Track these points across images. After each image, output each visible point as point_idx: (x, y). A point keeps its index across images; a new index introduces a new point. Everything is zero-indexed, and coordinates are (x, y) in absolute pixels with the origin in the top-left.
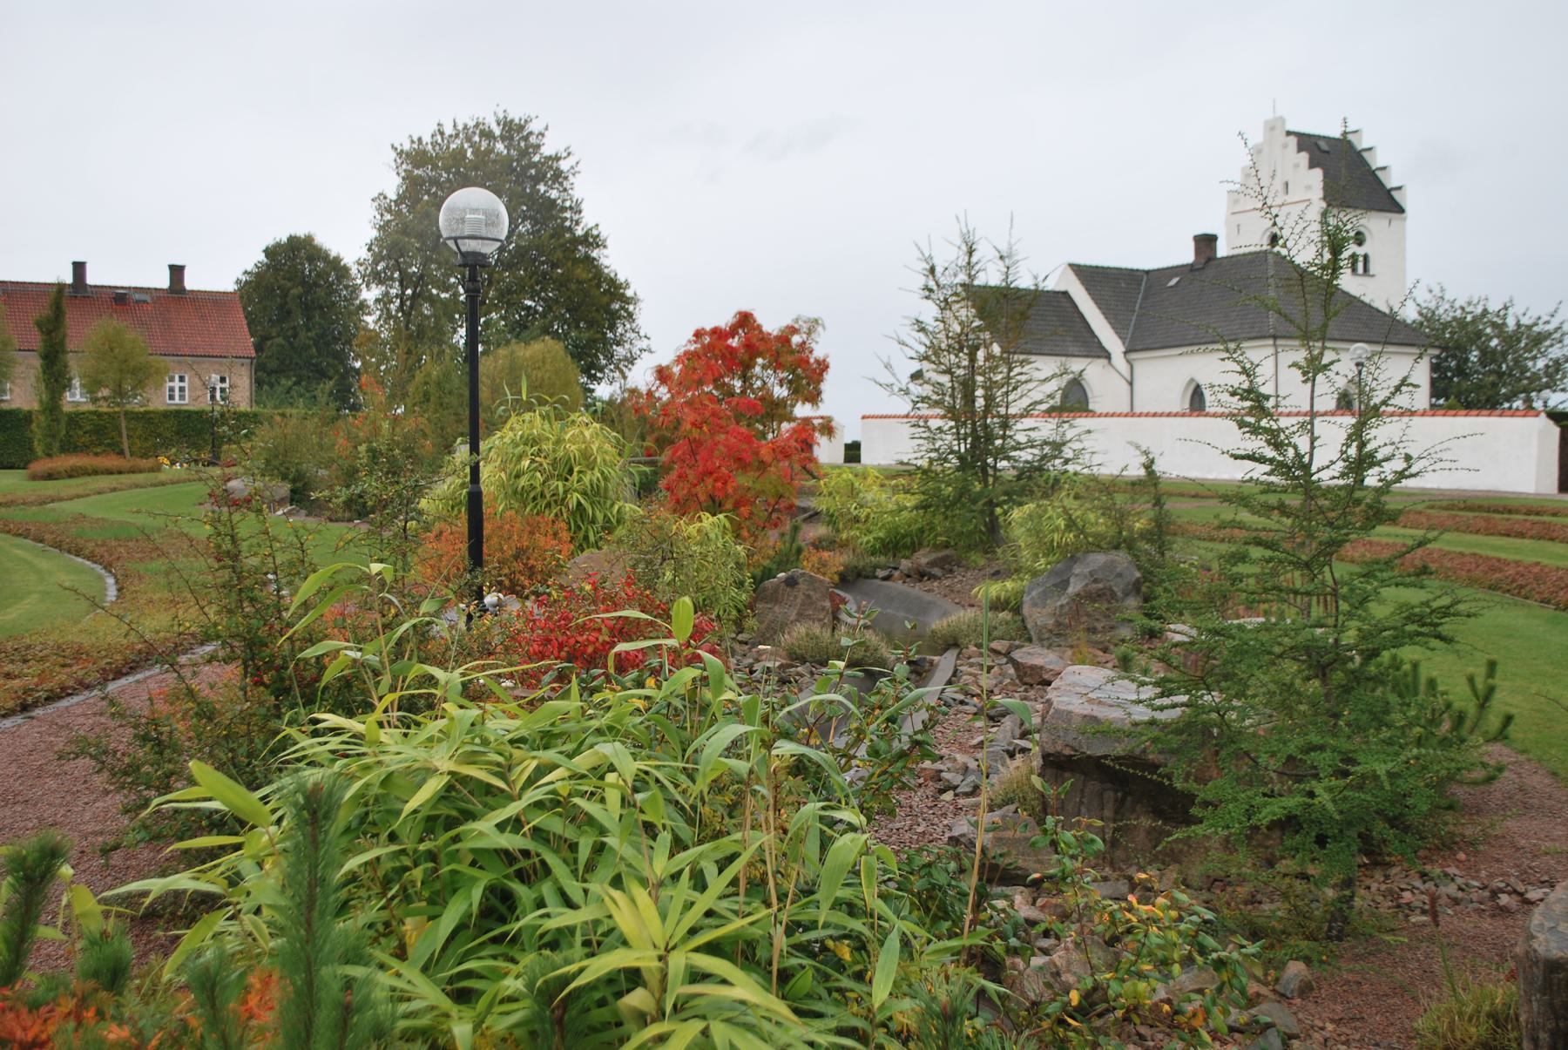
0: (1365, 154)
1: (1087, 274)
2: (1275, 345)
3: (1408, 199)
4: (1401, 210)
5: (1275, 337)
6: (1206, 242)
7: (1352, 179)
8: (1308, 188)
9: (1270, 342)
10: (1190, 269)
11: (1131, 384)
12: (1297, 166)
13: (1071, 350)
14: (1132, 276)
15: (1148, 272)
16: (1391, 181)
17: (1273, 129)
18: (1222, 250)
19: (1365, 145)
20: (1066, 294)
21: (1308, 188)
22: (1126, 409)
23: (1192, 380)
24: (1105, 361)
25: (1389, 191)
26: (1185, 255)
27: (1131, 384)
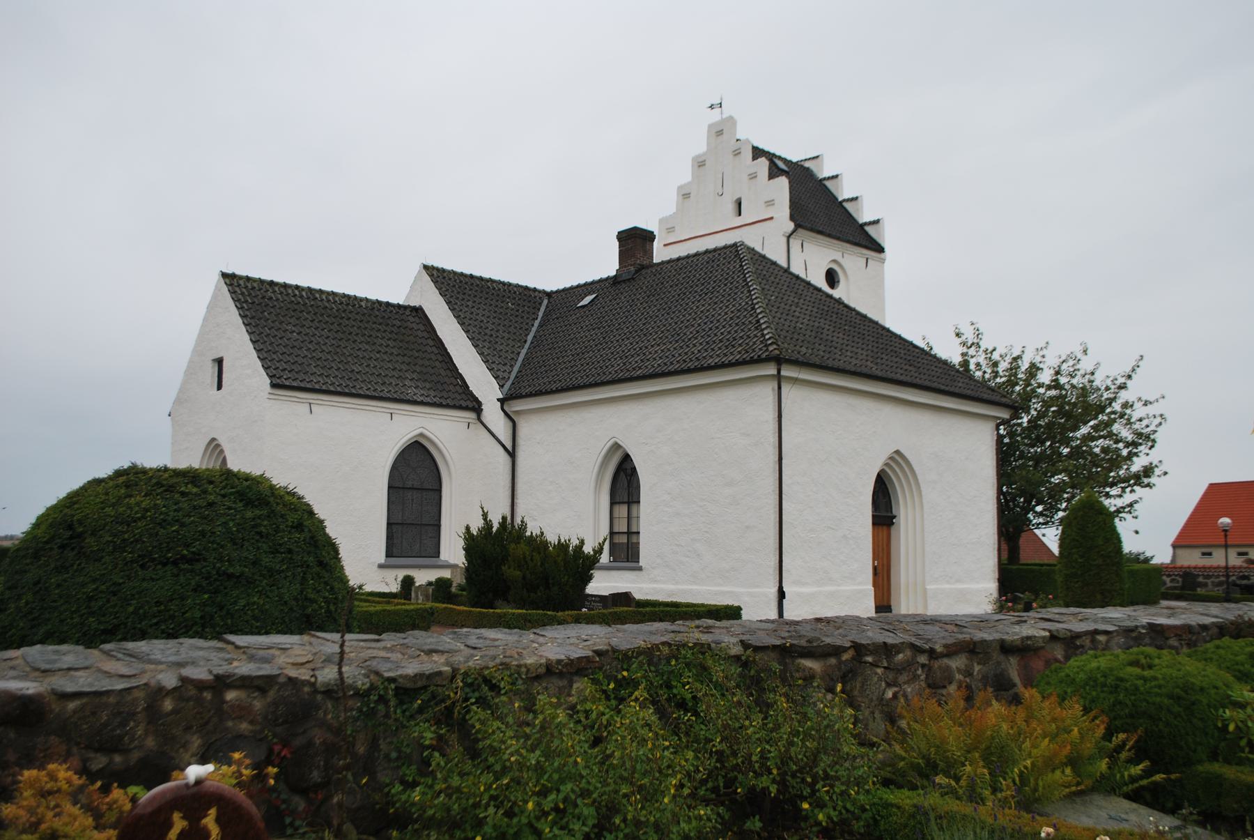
0: (828, 184)
1: (453, 285)
2: (779, 378)
3: (887, 237)
4: (880, 250)
5: (779, 361)
6: (634, 242)
7: (818, 206)
8: (770, 203)
9: (771, 370)
10: (614, 281)
11: (512, 454)
12: (753, 176)
13: (410, 392)
14: (526, 297)
15: (549, 295)
16: (864, 215)
17: (720, 133)
18: (660, 253)
19: (826, 174)
20: (418, 311)
21: (770, 203)
22: (616, 530)
23: (616, 446)
24: (471, 416)
25: (862, 226)
26: (607, 264)
27: (512, 454)
